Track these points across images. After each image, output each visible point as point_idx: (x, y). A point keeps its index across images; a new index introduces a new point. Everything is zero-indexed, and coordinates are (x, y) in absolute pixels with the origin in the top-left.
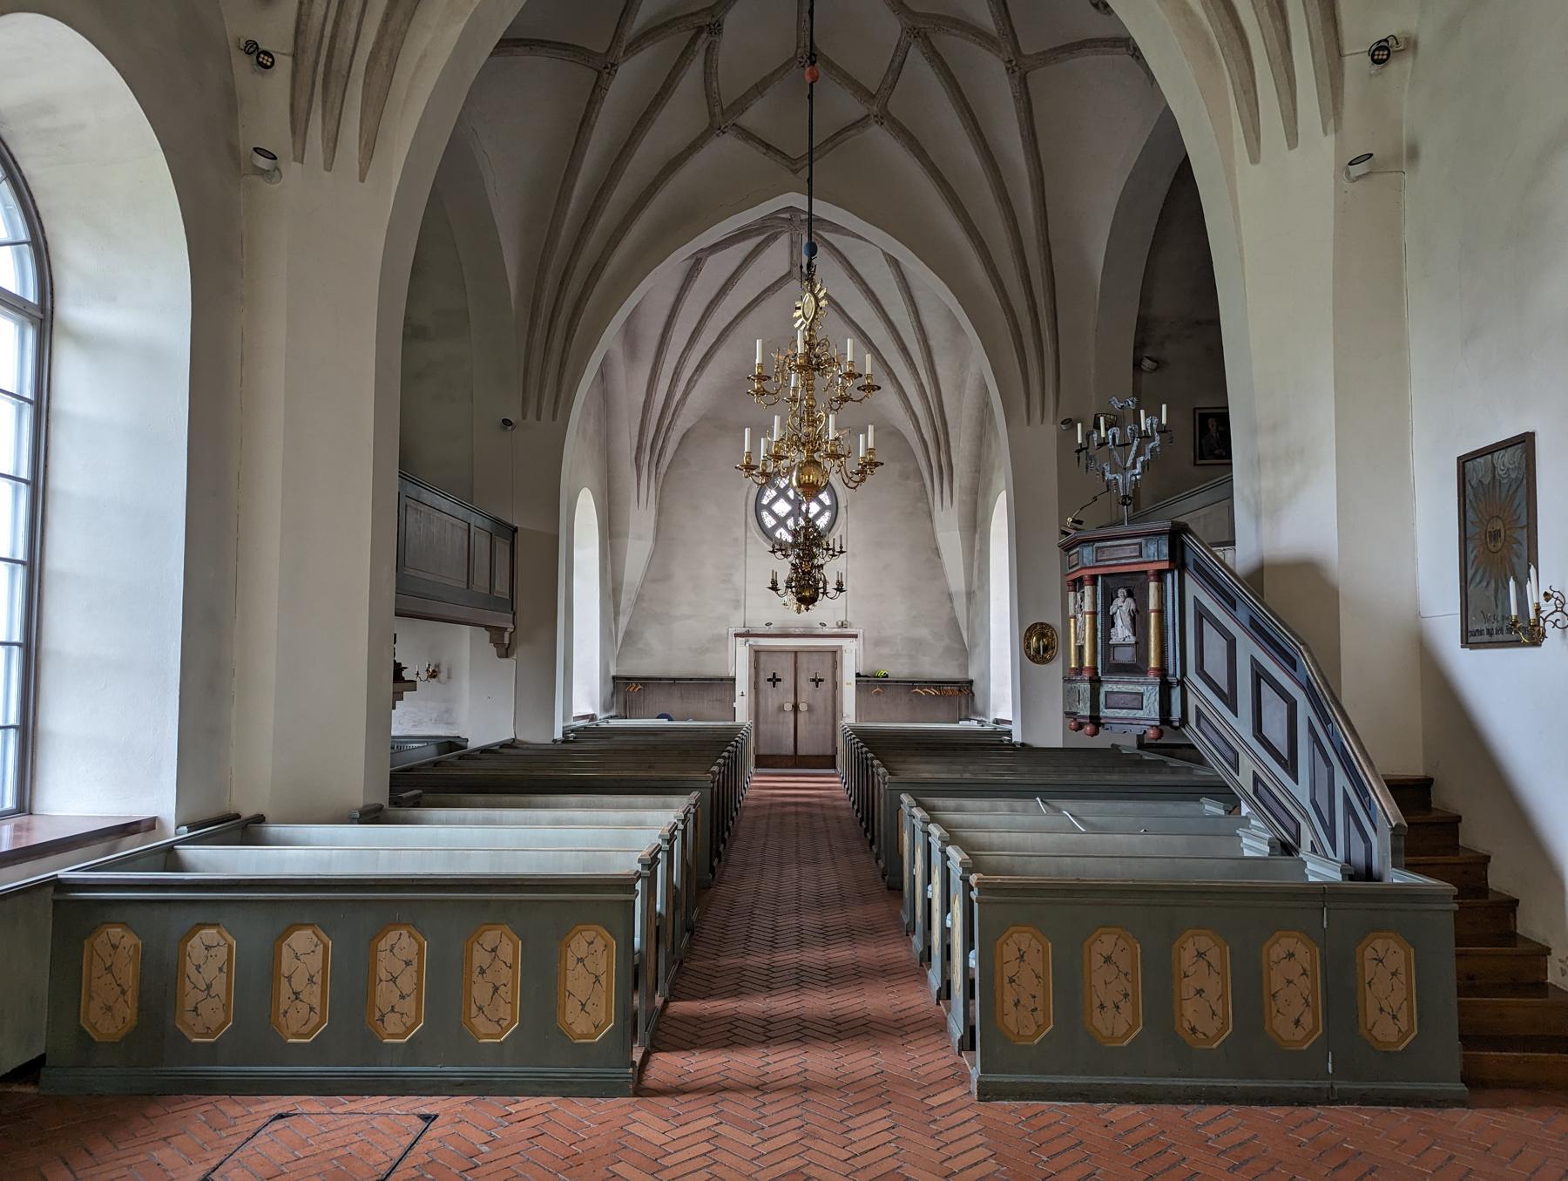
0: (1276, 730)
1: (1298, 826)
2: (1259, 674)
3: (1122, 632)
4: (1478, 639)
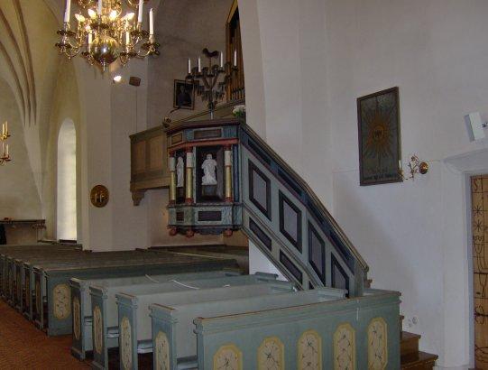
0: (291, 227)
1: (301, 274)
2: (282, 198)
3: (209, 179)
4: (369, 181)
